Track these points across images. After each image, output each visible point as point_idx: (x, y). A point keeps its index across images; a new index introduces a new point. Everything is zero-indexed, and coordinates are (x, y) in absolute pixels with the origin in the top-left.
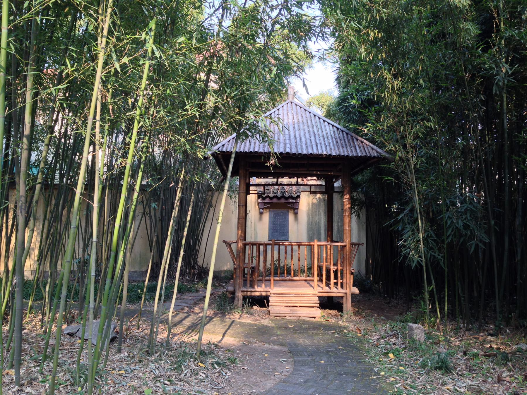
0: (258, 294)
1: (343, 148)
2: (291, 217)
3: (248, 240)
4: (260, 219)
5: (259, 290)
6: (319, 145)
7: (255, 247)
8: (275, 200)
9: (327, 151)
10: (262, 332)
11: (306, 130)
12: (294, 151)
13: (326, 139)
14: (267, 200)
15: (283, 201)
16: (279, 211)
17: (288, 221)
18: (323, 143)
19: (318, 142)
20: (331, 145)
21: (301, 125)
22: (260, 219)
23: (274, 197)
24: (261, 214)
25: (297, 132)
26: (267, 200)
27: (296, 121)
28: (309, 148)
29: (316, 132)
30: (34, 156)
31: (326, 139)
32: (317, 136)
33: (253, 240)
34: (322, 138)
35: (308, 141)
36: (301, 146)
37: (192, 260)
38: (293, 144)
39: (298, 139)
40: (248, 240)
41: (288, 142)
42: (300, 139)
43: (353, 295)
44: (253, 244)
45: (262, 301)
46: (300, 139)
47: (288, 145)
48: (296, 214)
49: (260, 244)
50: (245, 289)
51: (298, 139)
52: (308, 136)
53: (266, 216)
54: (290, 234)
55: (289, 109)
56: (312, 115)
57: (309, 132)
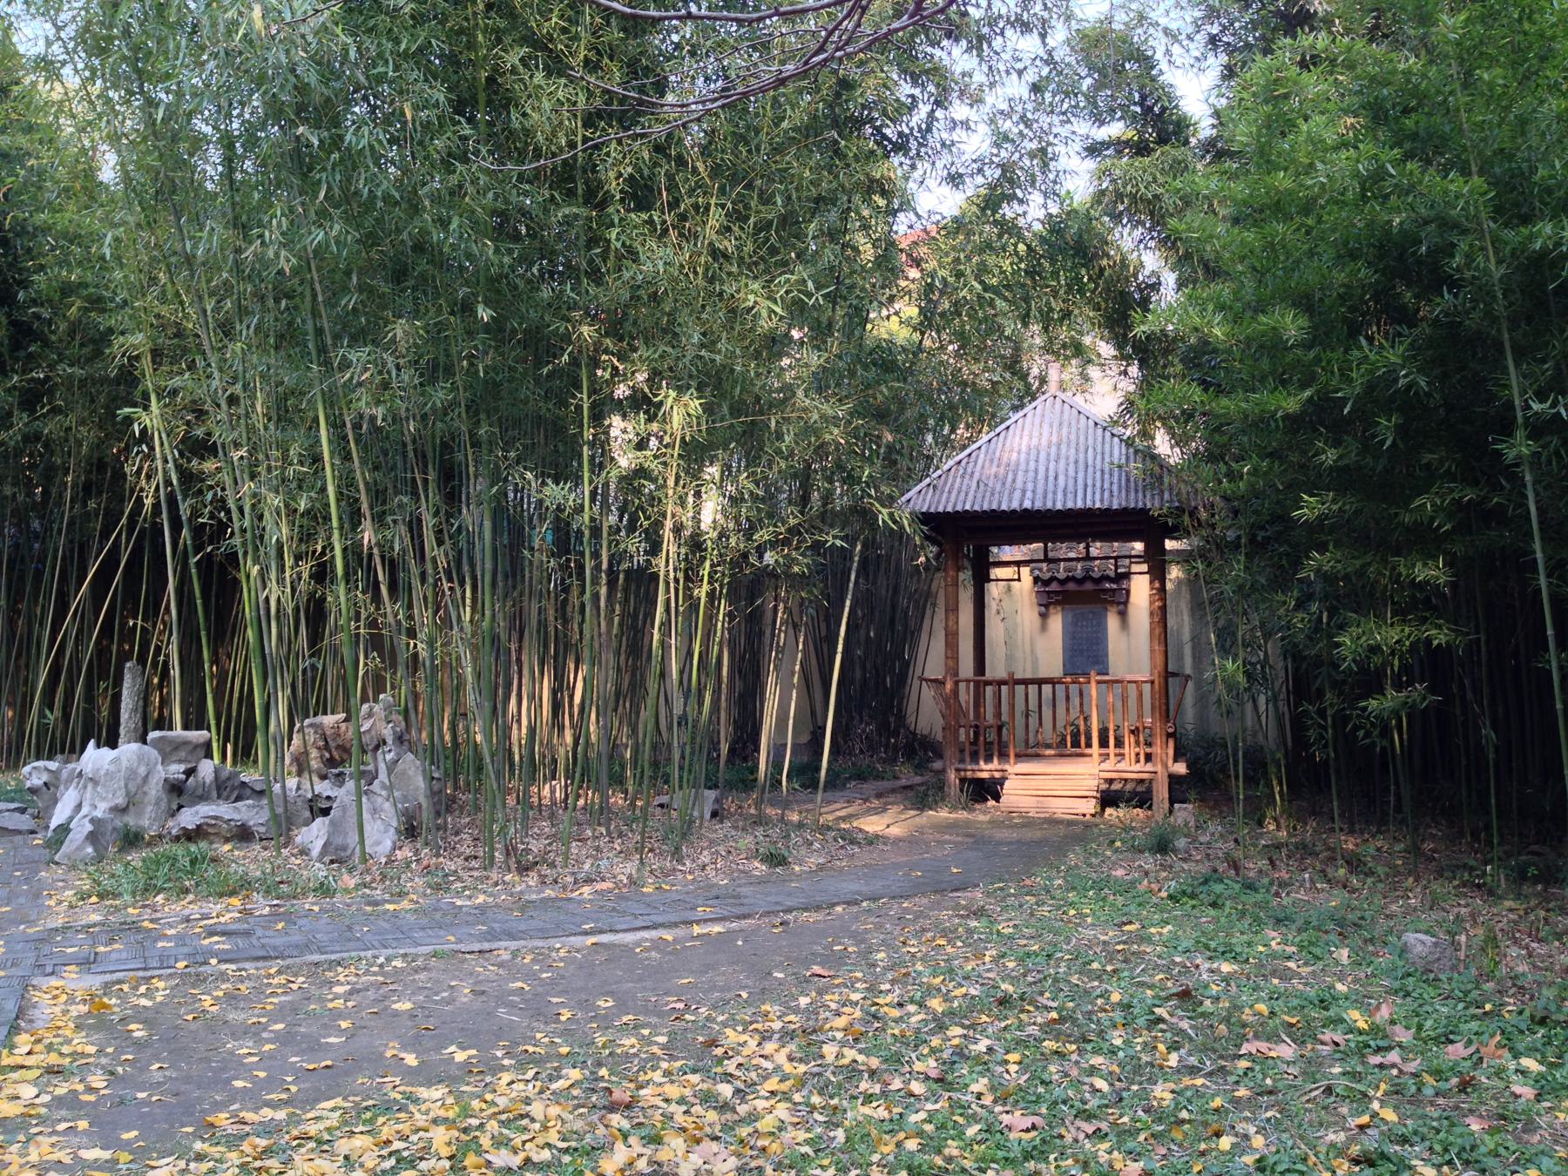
0: (985, 775)
1: (1137, 491)
2: (1112, 622)
3: (989, 675)
4: (1044, 627)
5: (986, 770)
6: (1089, 490)
7: (1004, 688)
8: (1071, 586)
9: (1102, 501)
10: (977, 840)
11: (1072, 460)
12: (1038, 505)
13: (1107, 476)
14: (1054, 587)
15: (1089, 586)
16: (1086, 609)
17: (1106, 629)
18: (1098, 484)
19: (1090, 482)
20: (1115, 488)
21: (1064, 447)
22: (1044, 627)
23: (1068, 579)
24: (1044, 616)
25: (1052, 466)
26: (1054, 587)
27: (1054, 439)
28: (1070, 496)
29: (1090, 462)
30: (581, 802)
31: (1107, 476)
32: (1090, 470)
33: (1029, 675)
34: (1098, 474)
35: (1071, 482)
36: (1055, 493)
37: (892, 719)
38: (1040, 491)
39: (1051, 479)
40: (989, 675)
41: (1030, 486)
42: (1056, 478)
43: (1174, 779)
44: (1000, 683)
45: (987, 790)
46: (1056, 478)
47: (1029, 494)
48: (1123, 614)
49: (1040, 682)
50: (961, 766)
51: (1051, 479)
52: (1071, 473)
53: (1056, 622)
54: (1111, 658)
55: (1047, 412)
56: (1091, 423)
57: (1076, 462)
